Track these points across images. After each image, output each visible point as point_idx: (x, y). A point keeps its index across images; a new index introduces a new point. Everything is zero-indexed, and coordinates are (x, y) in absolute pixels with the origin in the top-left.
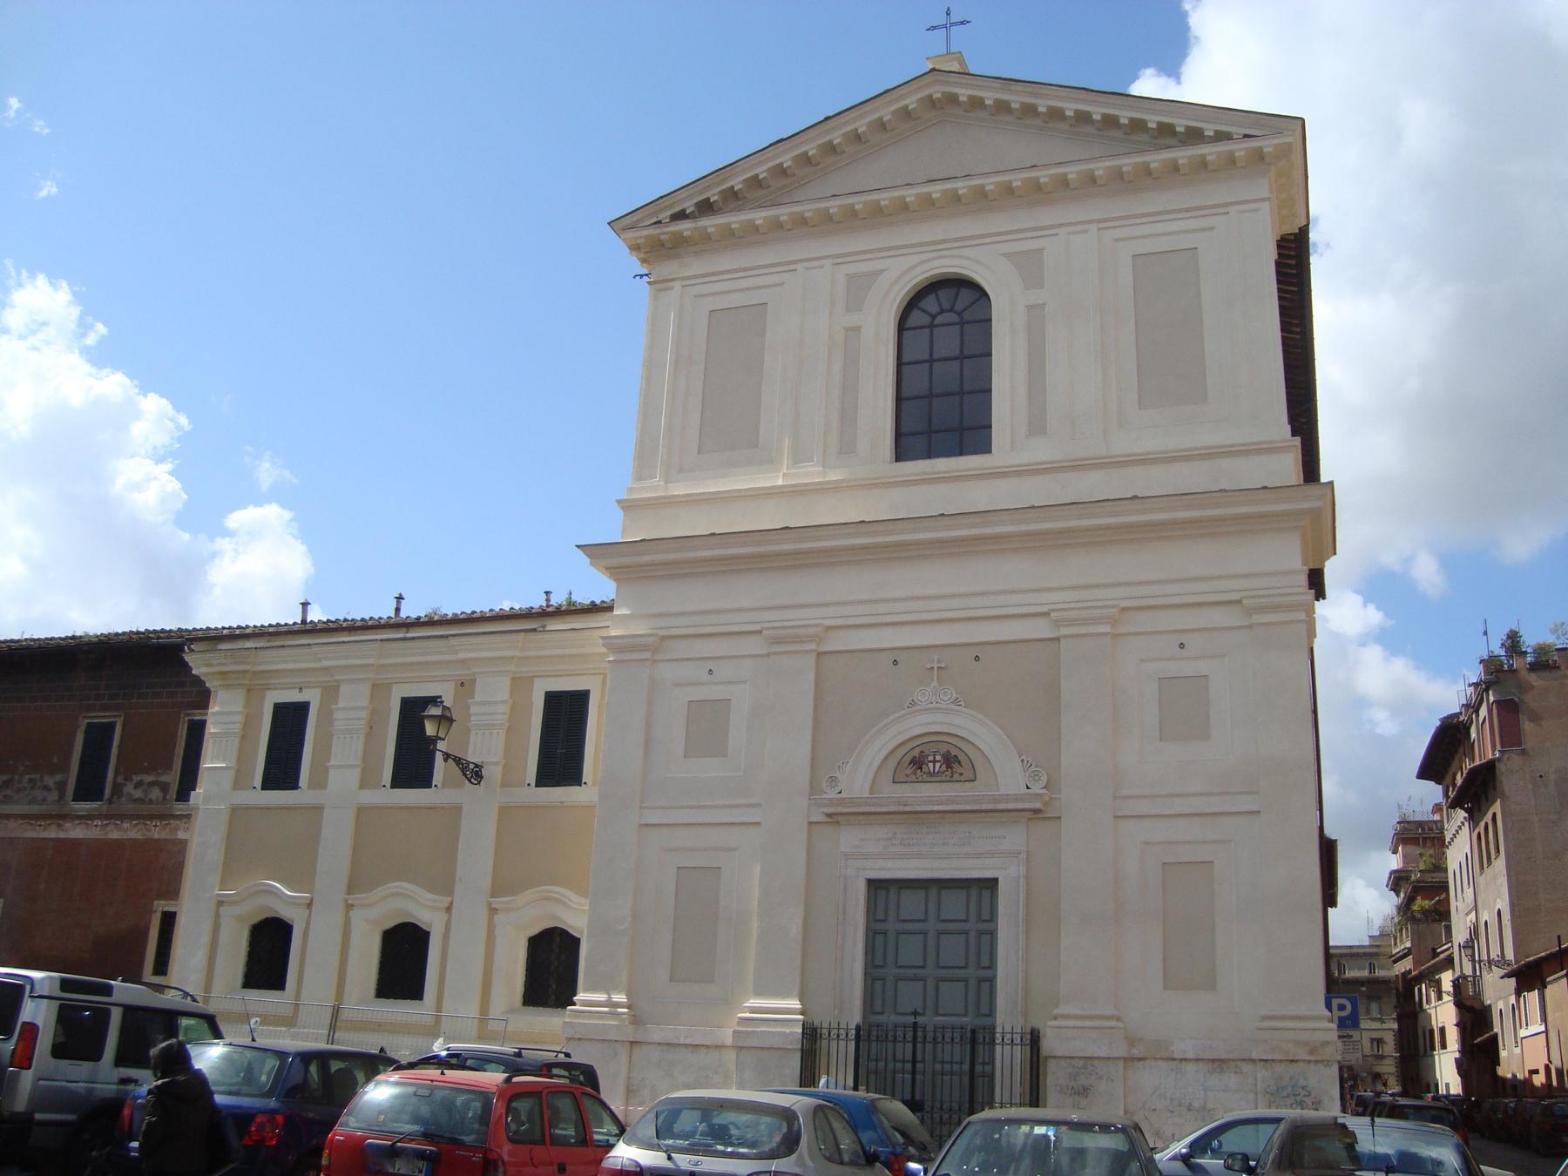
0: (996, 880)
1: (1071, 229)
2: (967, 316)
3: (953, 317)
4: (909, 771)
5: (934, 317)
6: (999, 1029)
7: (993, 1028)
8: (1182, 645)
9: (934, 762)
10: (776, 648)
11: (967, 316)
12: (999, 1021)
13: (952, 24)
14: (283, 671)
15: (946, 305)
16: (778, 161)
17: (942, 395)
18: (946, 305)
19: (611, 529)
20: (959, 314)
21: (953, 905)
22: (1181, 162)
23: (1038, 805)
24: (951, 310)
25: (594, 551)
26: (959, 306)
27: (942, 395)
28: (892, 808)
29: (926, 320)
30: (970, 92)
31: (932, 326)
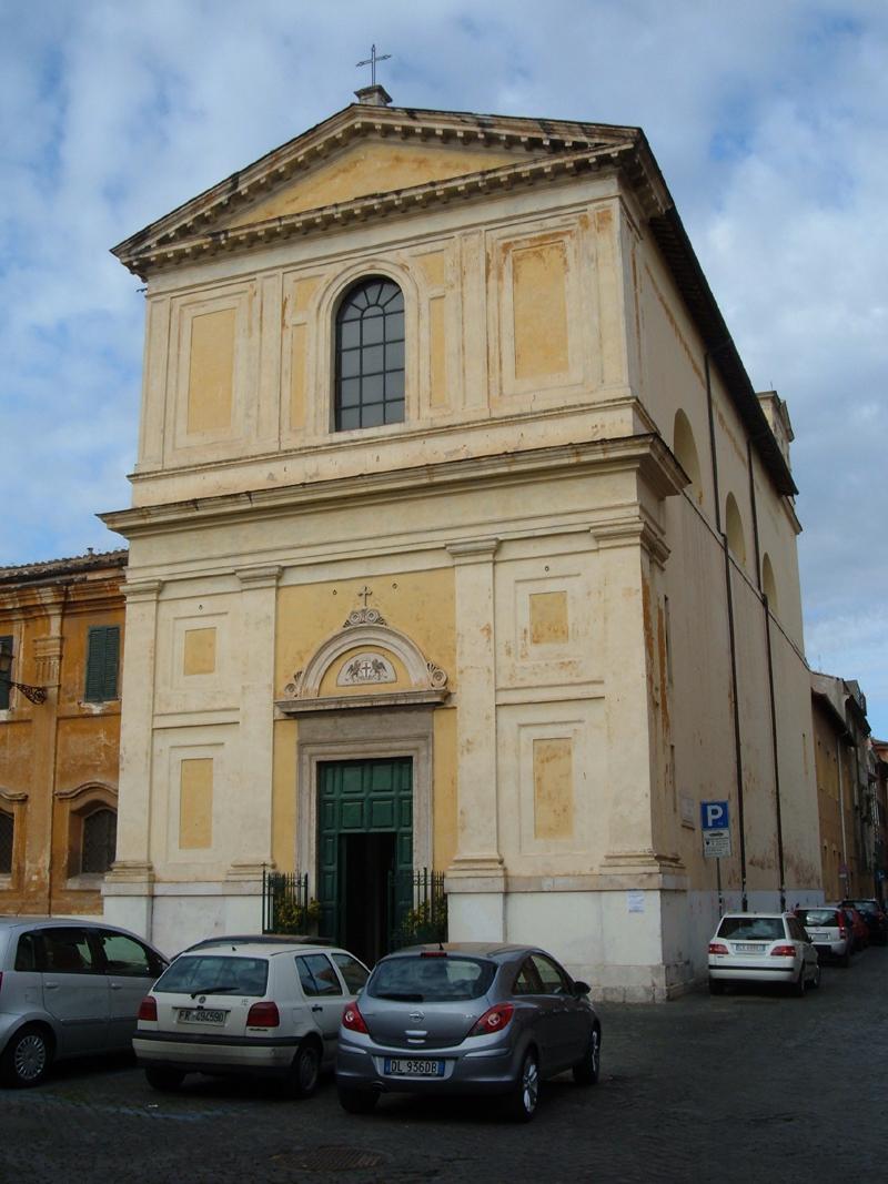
0: (411, 757)
1: (489, 227)
2: (389, 308)
3: (378, 310)
4: (348, 677)
5: (363, 311)
6: (416, 874)
7: (411, 871)
8: (547, 568)
9: (366, 668)
10: (246, 586)
11: (389, 308)
12: (414, 867)
13: (370, 61)
14: (660, 625)
15: (372, 301)
16: (331, 135)
17: (391, 371)
18: (372, 301)
19: (124, 497)
20: (383, 307)
21: (382, 777)
22: (612, 155)
23: (437, 699)
24: (377, 305)
25: (107, 517)
26: (381, 302)
27: (391, 371)
28: (333, 707)
29: (357, 314)
30: (209, 207)
31: (361, 319)
